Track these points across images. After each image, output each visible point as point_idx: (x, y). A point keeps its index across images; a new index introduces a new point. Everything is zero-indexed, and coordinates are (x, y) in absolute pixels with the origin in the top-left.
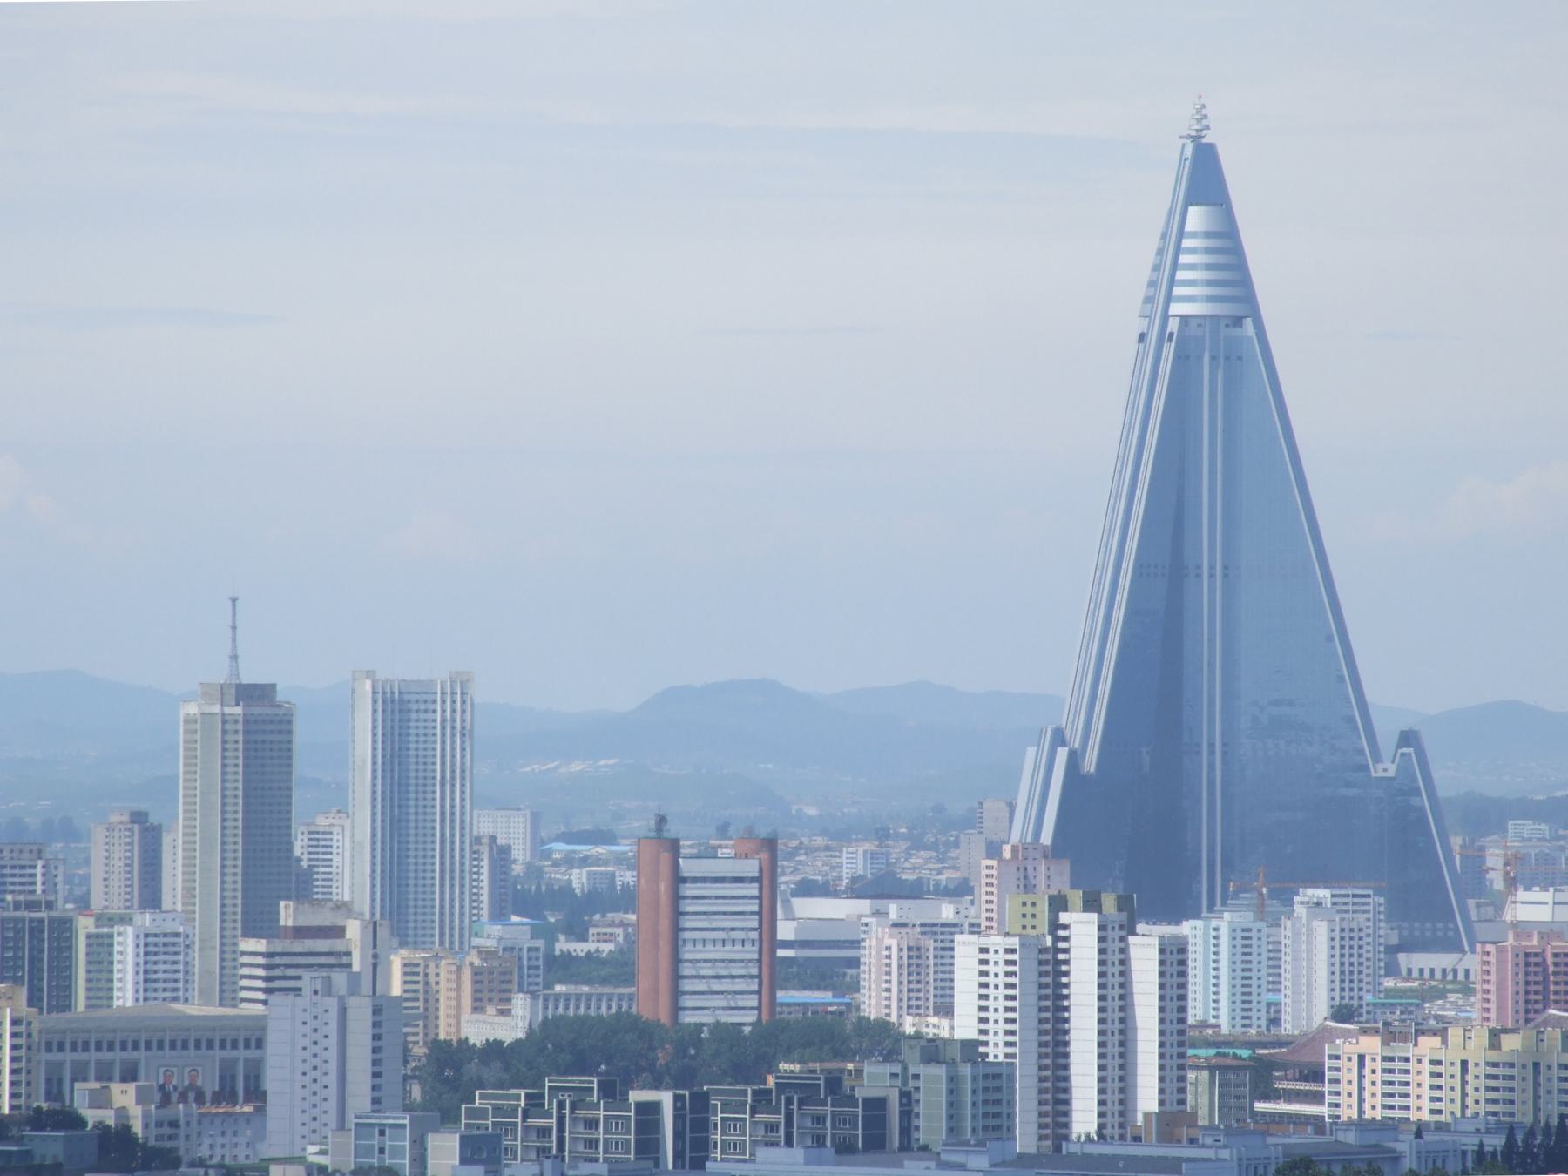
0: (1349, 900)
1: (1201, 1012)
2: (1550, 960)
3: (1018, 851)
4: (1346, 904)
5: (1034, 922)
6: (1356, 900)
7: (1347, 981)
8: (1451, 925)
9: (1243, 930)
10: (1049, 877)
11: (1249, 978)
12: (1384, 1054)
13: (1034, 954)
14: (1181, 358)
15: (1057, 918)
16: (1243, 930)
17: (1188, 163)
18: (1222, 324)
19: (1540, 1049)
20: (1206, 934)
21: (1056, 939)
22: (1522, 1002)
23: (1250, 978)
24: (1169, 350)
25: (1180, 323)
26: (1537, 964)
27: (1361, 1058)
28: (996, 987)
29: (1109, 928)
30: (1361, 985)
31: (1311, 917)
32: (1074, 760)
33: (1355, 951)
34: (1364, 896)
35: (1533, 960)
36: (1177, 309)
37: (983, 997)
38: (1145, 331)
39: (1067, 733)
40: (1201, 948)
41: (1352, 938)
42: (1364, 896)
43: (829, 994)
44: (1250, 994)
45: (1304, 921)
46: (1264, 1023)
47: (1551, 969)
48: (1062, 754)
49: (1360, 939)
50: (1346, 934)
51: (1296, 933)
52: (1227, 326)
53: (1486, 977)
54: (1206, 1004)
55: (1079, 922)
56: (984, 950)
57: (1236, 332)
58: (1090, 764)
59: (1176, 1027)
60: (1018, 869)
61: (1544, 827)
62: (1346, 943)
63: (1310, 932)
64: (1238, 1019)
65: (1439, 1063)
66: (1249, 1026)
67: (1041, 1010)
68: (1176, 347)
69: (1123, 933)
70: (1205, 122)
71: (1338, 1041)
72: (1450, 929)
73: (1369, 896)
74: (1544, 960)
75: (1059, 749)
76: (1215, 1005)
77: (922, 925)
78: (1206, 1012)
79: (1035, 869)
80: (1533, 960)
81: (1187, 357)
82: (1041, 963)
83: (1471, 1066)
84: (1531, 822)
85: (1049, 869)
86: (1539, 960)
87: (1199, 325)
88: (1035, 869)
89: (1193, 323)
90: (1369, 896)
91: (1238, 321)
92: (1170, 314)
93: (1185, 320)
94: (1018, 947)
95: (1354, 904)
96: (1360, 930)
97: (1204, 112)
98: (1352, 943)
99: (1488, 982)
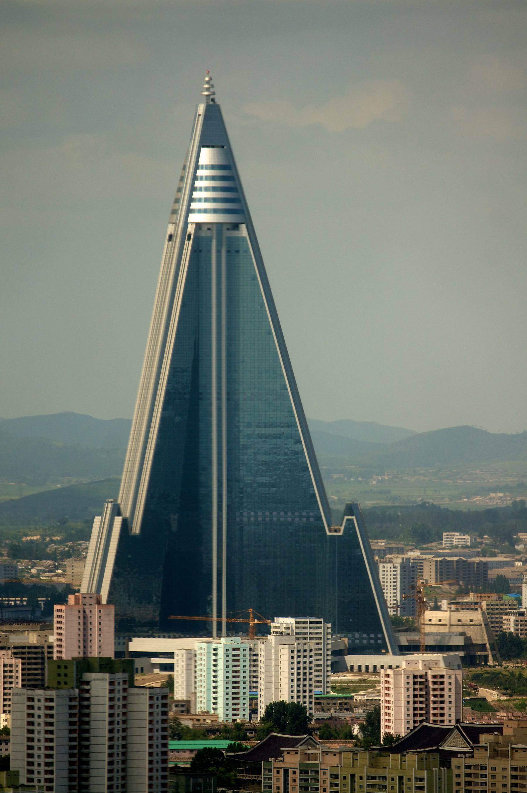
0: (308, 625)
1: (205, 706)
2: (430, 679)
3: (79, 599)
5: (66, 679)
6: (312, 625)
7: (302, 686)
8: (380, 636)
10: (100, 617)
11: (238, 682)
12: (301, 769)
13: (67, 702)
14: (196, 251)
17: (201, 119)
18: (225, 227)
19: (403, 768)
20: (208, 653)
21: (82, 691)
22: (411, 709)
23: (238, 682)
24: (189, 245)
26: (421, 683)
27: (286, 771)
28: (39, 724)
29: (116, 683)
30: (311, 688)
31: (278, 643)
32: (126, 525)
33: (307, 665)
34: (317, 623)
36: (194, 218)
37: (31, 723)
38: (173, 233)
42: (317, 623)
45: (273, 645)
46: (247, 712)
47: (431, 686)
48: (118, 520)
50: (301, 654)
51: (268, 654)
52: (228, 229)
53: (387, 692)
54: (208, 700)
55: (98, 679)
56: (31, 699)
57: (235, 233)
58: (136, 528)
59: (161, 749)
60: (79, 612)
61: (467, 537)
62: (302, 660)
63: (277, 653)
64: (230, 710)
65: (336, 776)
66: (238, 715)
69: (126, 686)
71: (270, 760)
72: (379, 639)
73: (321, 622)
75: (116, 518)
76: (214, 701)
77: (15, 648)
78: (208, 706)
79: (91, 611)
81: (201, 251)
82: (71, 707)
83: (357, 779)
84: (458, 534)
85: (100, 611)
86: (423, 680)
88: (91, 611)
89: (205, 228)
90: (321, 622)
91: (236, 226)
92: (189, 221)
93: (199, 226)
95: (311, 628)
96: (311, 651)
98: (305, 660)
99: (388, 695)
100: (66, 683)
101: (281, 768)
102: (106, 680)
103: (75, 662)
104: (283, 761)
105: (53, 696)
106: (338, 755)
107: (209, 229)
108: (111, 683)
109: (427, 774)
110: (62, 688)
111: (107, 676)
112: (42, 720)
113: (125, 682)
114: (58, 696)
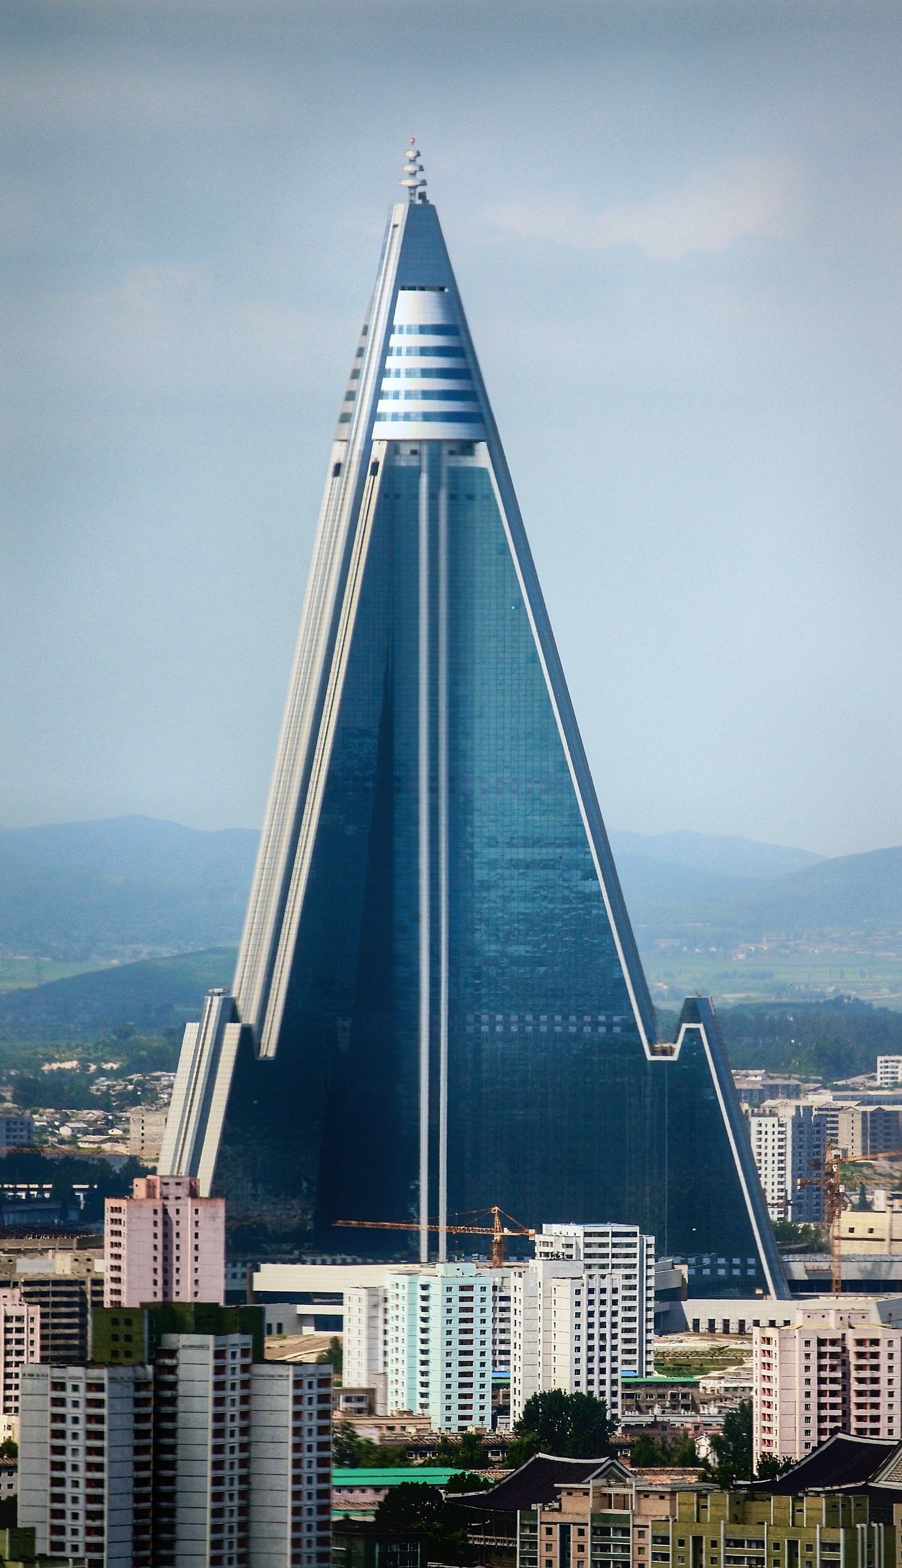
2: (852, 1348)
3: (154, 1187)
4: (602, 1245)
6: (617, 1240)
7: (596, 1360)
8: (751, 1261)
9: (462, 1288)
10: (197, 1223)
12: (595, 1524)
15: (159, 1342)
16: (462, 1288)
18: (445, 450)
24: (374, 484)
25: (388, 450)
26: (833, 1355)
27: (565, 1529)
29: (229, 1355)
30: (615, 1365)
34: (627, 1235)
35: (828, 1349)
36: (385, 431)
38: (342, 461)
39: (240, 1004)
40: (406, 1313)
41: (603, 1302)
42: (627, 1235)
43: (192, 1029)
44: (470, 1374)
47: (853, 1360)
48: (233, 1032)
49: (615, 1302)
52: (452, 453)
56: (58, 1386)
58: (269, 1047)
59: (315, 1486)
62: (596, 1308)
67: (138, 1466)
68: (382, 483)
69: (248, 1360)
70: (420, 176)
71: (534, 1506)
72: (751, 1267)
73: (634, 1234)
74: (844, 1349)
77: (27, 1283)
78: (411, 1400)
80: (828, 1349)
85: (197, 1211)
87: (414, 452)
89: (405, 450)
90: (634, 1234)
91: (466, 447)
92: (374, 437)
93: (394, 446)
94: (106, 1382)
95: (615, 1245)
97: (419, 161)
100: (128, 1354)
101: (555, 1523)
102: (208, 1348)
103: (146, 1312)
104: (559, 1510)
105: (103, 1379)
106: (667, 1497)
107: (414, 452)
108: (219, 1354)
109: (846, 1535)
110: (120, 1364)
111: (210, 1340)
112: (80, 1428)
113: (245, 1353)
114: (112, 1379)
